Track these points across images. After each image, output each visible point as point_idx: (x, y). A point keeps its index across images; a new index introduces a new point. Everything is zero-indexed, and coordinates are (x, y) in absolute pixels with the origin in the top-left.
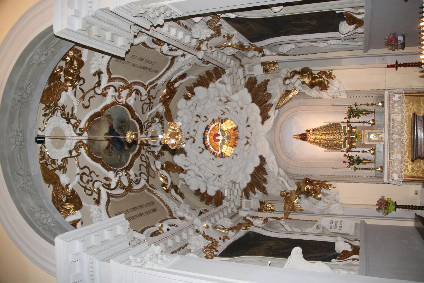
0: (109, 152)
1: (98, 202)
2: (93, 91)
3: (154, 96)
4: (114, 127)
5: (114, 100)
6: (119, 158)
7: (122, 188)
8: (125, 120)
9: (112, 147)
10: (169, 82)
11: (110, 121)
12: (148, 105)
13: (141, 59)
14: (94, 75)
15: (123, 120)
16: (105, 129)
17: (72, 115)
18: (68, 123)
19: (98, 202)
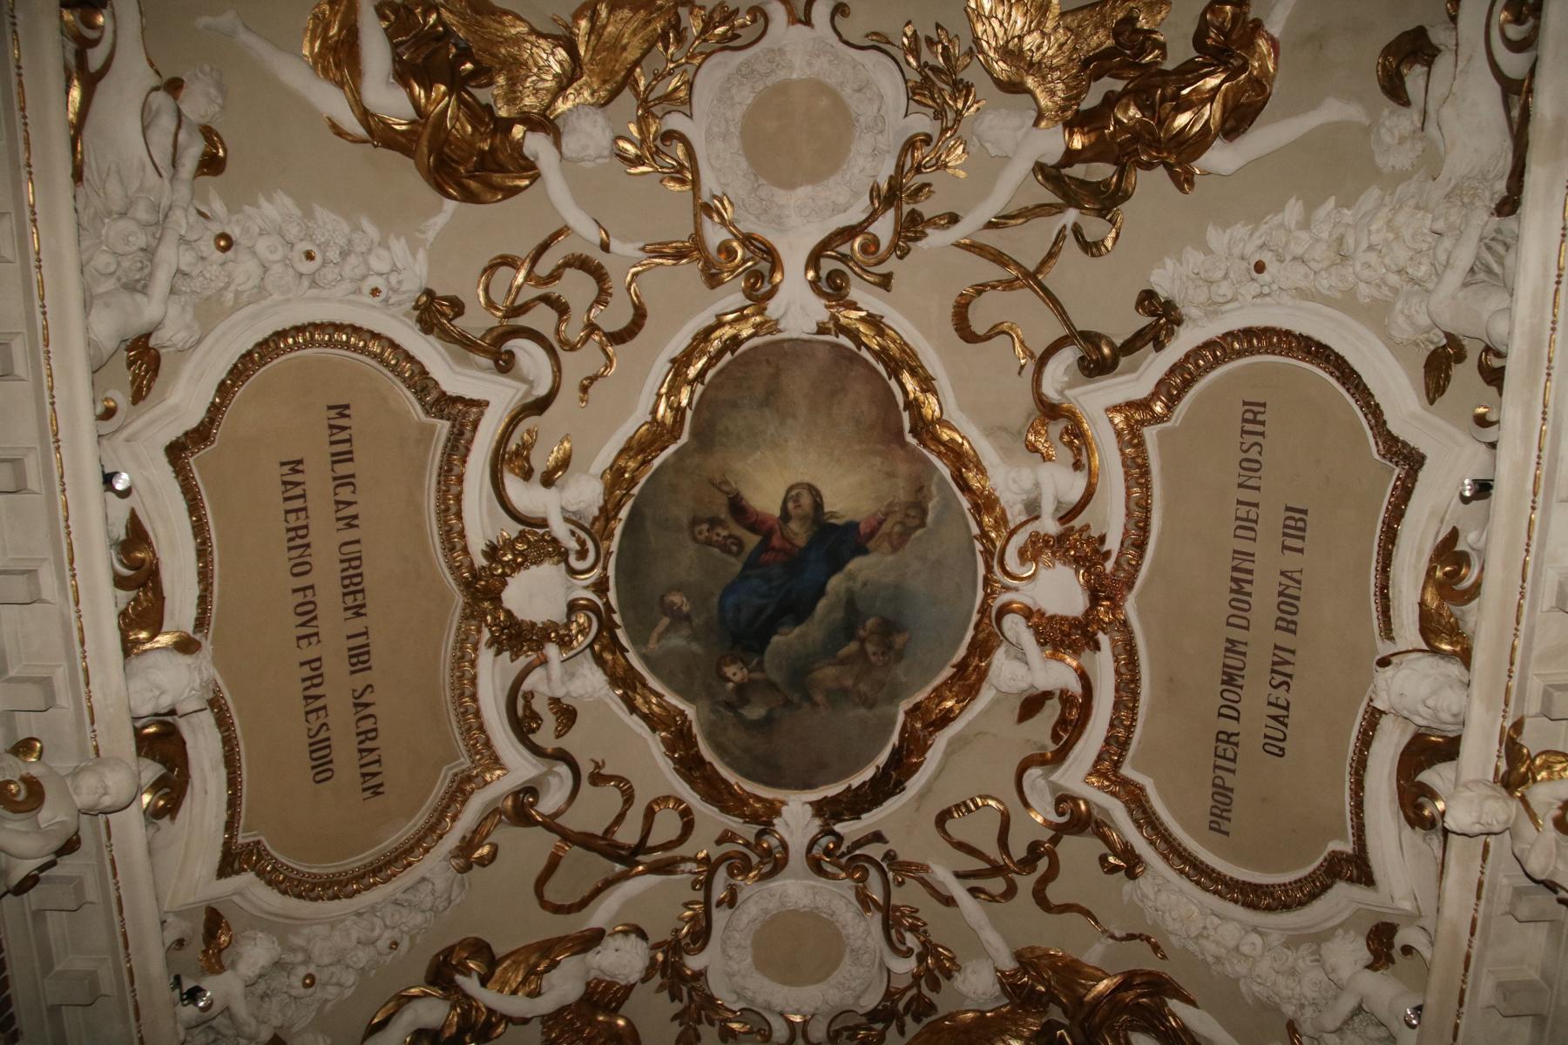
0: (714, 522)
1: (434, 313)
2: (1062, 331)
3: (1055, 893)
4: (854, 564)
5: (1012, 504)
6: (676, 599)
7: (492, 552)
8: (900, 656)
9: (740, 543)
10: (1160, 986)
11: (886, 527)
12: (993, 852)
13: (1288, 601)
14: (1147, 299)
15: (899, 640)
16: (848, 492)
17: (915, 219)
18: (874, 191)
19: (434, 313)
